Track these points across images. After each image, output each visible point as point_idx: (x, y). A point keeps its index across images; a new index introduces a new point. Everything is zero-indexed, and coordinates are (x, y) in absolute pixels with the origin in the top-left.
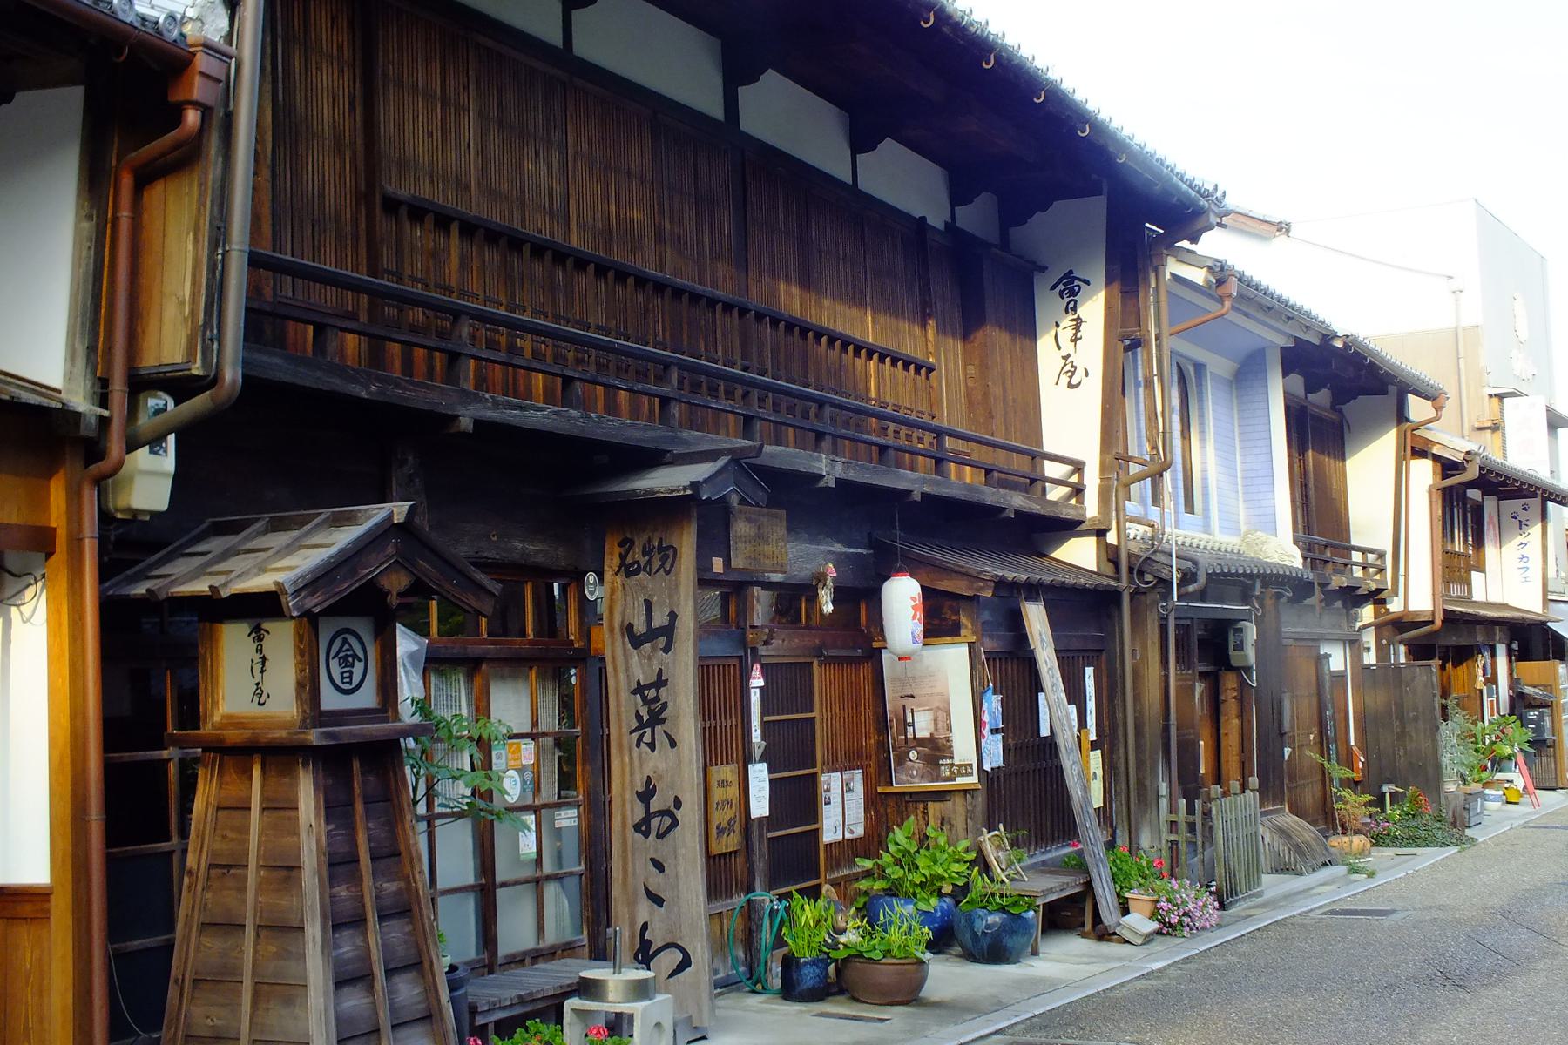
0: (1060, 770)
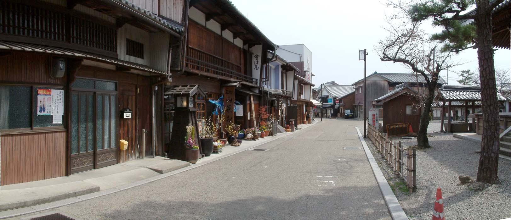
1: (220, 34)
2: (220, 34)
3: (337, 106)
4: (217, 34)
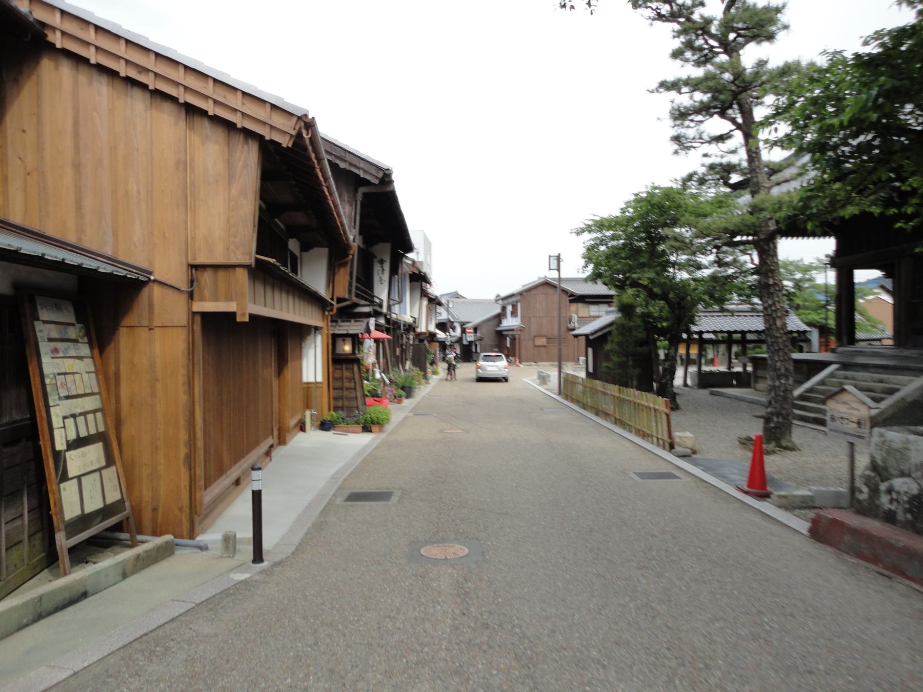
3: (470, 337)
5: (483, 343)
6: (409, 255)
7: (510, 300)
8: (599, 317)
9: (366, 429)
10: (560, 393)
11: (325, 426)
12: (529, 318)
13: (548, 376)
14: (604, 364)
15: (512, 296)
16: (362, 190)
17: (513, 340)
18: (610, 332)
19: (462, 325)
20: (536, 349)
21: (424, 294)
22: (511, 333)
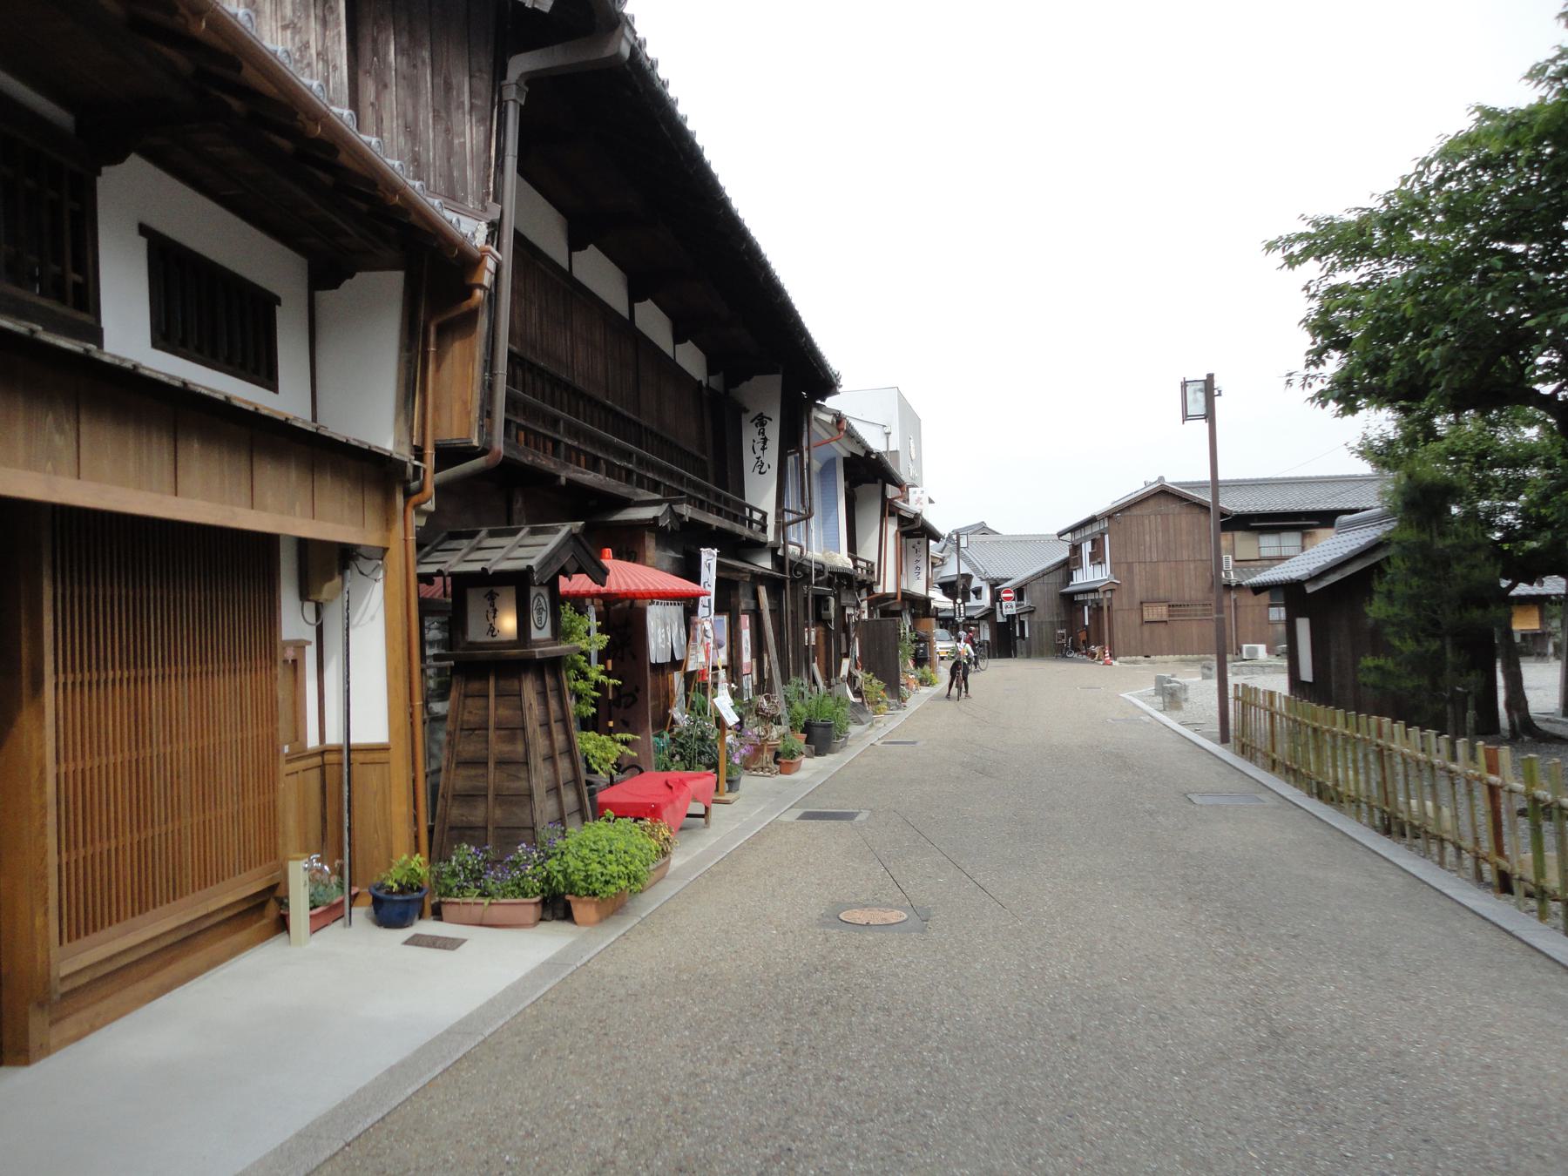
0: (1161, 654)
1: (625, 313)
2: (625, 313)
3: (1009, 608)
4: (620, 316)
5: (1035, 618)
6: (831, 402)
7: (1088, 531)
8: (1282, 559)
9: (556, 905)
10: (1224, 738)
11: (393, 910)
12: (1130, 565)
13: (1184, 688)
14: (1368, 662)
15: (1092, 521)
16: (520, 65)
17: (1097, 610)
18: (1377, 569)
19: (994, 585)
20: (1146, 627)
21: (889, 509)
22: (1091, 596)
